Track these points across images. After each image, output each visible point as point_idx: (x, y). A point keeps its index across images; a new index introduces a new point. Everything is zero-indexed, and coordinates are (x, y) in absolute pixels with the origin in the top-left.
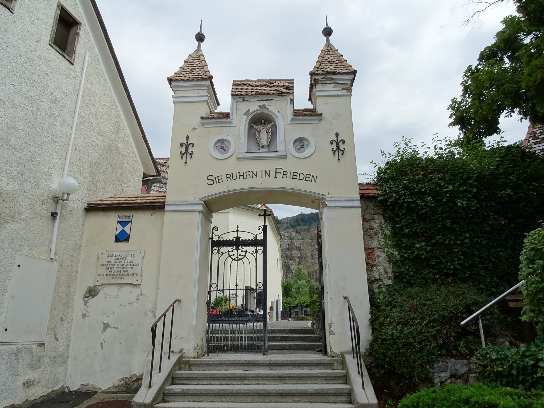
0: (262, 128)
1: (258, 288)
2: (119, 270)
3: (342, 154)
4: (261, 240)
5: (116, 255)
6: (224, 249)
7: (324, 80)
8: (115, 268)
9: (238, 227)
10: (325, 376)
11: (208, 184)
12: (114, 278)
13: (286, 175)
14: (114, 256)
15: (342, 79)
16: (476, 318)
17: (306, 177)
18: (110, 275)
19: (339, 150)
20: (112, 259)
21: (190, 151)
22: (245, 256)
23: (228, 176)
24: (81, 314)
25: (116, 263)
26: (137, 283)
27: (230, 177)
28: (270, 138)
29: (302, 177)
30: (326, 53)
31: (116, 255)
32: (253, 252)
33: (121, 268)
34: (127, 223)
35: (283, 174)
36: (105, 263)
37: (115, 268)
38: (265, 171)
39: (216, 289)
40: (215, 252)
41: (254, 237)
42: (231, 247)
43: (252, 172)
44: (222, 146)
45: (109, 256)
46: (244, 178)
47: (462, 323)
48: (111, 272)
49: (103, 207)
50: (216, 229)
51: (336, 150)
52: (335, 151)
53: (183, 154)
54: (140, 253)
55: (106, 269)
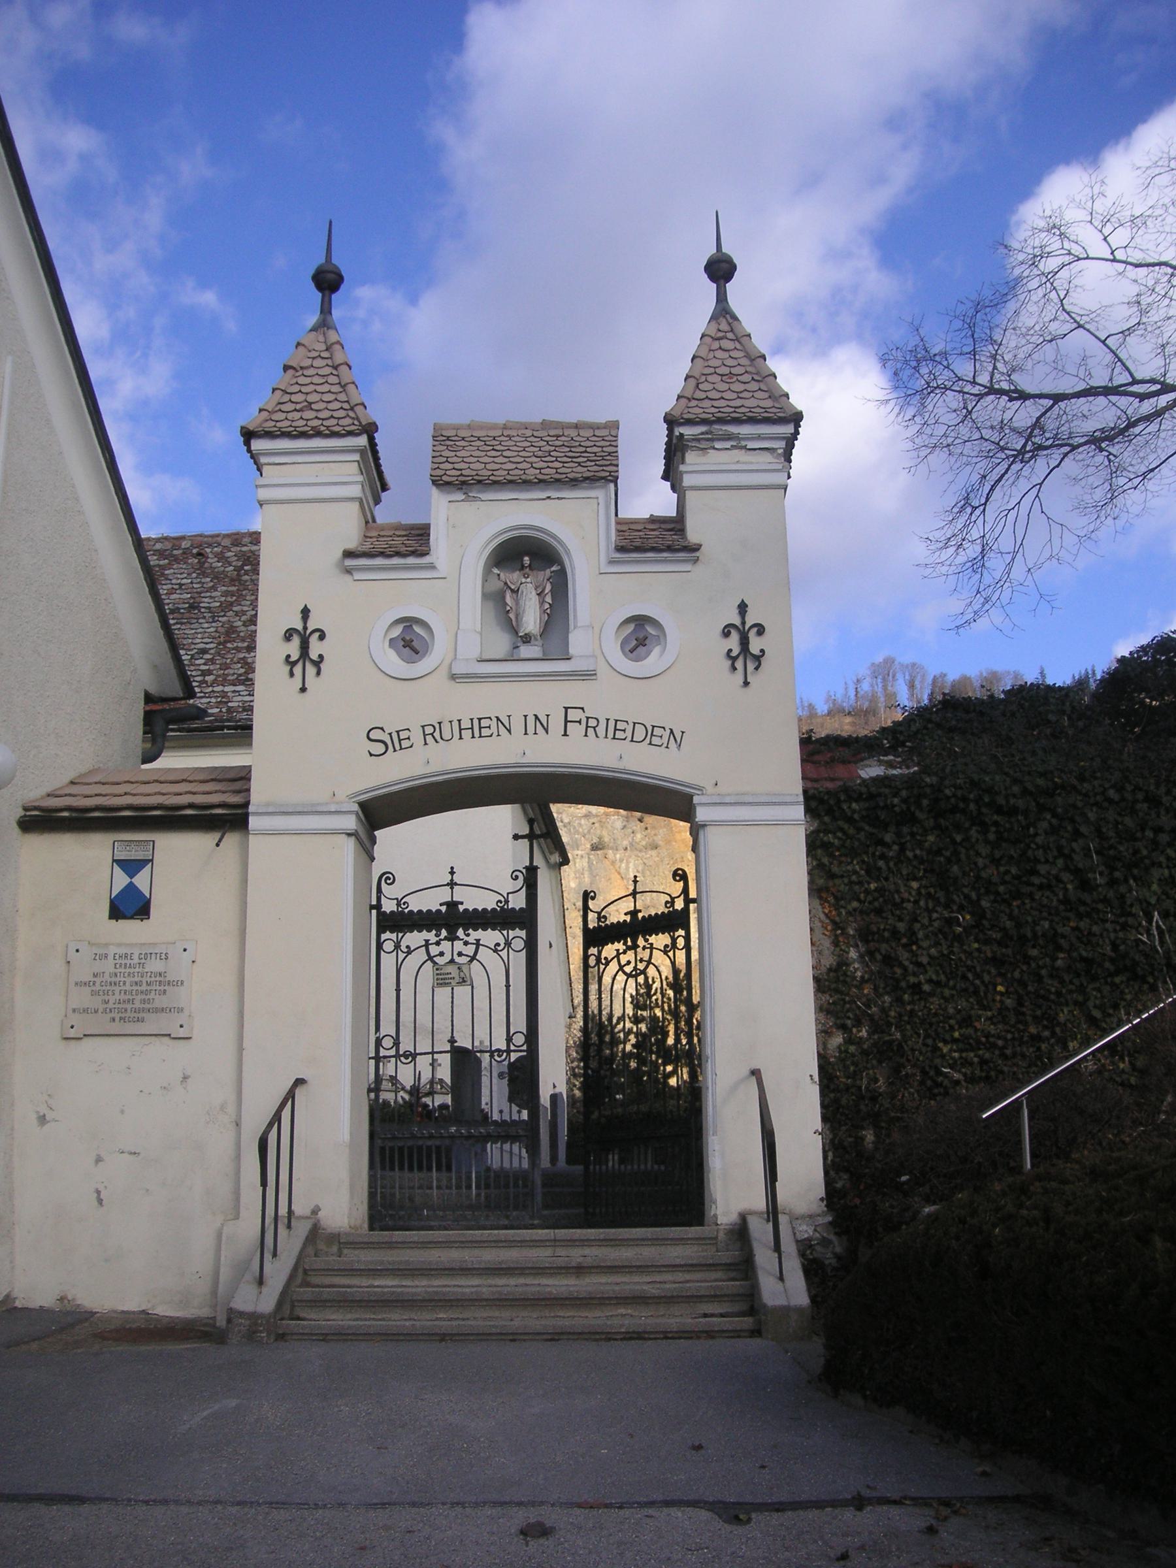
0: (524, 580)
1: (512, 1048)
2: (127, 997)
3: (757, 668)
4: (521, 909)
5: (117, 956)
6: (414, 938)
7: (708, 440)
8: (117, 992)
9: (452, 873)
10: (695, 1262)
11: (371, 755)
12: (117, 1019)
13: (594, 728)
14: (111, 957)
15: (760, 437)
16: (1016, 1106)
17: (652, 735)
18: (105, 1011)
19: (748, 655)
20: (108, 966)
21: (314, 655)
22: (473, 958)
23: (429, 730)
24: (35, 1116)
25: (118, 979)
26: (182, 1033)
27: (433, 733)
28: (548, 611)
29: (640, 733)
30: (716, 345)
31: (117, 956)
32: (498, 944)
33: (134, 993)
34: (142, 863)
35: (587, 727)
36: (88, 978)
37: (117, 992)
38: (535, 715)
39: (393, 1052)
40: (388, 946)
41: (501, 902)
42: (434, 932)
43: (498, 719)
44: (408, 638)
45: (97, 958)
46: (473, 737)
47: (984, 1116)
48: (107, 1002)
49: (64, 818)
50: (388, 878)
51: (738, 656)
52: (734, 659)
53: (294, 664)
54: (185, 950)
55: (93, 993)
